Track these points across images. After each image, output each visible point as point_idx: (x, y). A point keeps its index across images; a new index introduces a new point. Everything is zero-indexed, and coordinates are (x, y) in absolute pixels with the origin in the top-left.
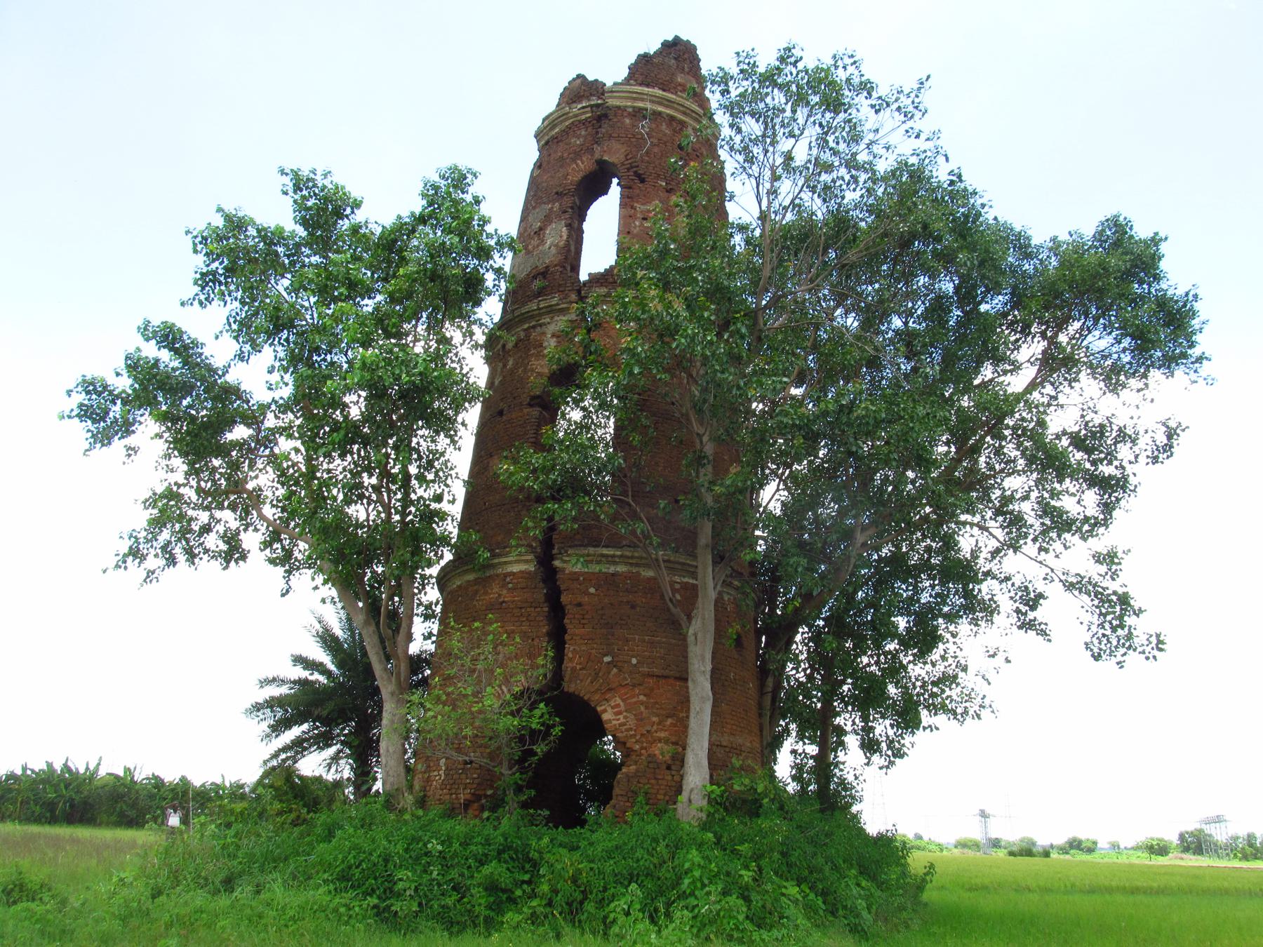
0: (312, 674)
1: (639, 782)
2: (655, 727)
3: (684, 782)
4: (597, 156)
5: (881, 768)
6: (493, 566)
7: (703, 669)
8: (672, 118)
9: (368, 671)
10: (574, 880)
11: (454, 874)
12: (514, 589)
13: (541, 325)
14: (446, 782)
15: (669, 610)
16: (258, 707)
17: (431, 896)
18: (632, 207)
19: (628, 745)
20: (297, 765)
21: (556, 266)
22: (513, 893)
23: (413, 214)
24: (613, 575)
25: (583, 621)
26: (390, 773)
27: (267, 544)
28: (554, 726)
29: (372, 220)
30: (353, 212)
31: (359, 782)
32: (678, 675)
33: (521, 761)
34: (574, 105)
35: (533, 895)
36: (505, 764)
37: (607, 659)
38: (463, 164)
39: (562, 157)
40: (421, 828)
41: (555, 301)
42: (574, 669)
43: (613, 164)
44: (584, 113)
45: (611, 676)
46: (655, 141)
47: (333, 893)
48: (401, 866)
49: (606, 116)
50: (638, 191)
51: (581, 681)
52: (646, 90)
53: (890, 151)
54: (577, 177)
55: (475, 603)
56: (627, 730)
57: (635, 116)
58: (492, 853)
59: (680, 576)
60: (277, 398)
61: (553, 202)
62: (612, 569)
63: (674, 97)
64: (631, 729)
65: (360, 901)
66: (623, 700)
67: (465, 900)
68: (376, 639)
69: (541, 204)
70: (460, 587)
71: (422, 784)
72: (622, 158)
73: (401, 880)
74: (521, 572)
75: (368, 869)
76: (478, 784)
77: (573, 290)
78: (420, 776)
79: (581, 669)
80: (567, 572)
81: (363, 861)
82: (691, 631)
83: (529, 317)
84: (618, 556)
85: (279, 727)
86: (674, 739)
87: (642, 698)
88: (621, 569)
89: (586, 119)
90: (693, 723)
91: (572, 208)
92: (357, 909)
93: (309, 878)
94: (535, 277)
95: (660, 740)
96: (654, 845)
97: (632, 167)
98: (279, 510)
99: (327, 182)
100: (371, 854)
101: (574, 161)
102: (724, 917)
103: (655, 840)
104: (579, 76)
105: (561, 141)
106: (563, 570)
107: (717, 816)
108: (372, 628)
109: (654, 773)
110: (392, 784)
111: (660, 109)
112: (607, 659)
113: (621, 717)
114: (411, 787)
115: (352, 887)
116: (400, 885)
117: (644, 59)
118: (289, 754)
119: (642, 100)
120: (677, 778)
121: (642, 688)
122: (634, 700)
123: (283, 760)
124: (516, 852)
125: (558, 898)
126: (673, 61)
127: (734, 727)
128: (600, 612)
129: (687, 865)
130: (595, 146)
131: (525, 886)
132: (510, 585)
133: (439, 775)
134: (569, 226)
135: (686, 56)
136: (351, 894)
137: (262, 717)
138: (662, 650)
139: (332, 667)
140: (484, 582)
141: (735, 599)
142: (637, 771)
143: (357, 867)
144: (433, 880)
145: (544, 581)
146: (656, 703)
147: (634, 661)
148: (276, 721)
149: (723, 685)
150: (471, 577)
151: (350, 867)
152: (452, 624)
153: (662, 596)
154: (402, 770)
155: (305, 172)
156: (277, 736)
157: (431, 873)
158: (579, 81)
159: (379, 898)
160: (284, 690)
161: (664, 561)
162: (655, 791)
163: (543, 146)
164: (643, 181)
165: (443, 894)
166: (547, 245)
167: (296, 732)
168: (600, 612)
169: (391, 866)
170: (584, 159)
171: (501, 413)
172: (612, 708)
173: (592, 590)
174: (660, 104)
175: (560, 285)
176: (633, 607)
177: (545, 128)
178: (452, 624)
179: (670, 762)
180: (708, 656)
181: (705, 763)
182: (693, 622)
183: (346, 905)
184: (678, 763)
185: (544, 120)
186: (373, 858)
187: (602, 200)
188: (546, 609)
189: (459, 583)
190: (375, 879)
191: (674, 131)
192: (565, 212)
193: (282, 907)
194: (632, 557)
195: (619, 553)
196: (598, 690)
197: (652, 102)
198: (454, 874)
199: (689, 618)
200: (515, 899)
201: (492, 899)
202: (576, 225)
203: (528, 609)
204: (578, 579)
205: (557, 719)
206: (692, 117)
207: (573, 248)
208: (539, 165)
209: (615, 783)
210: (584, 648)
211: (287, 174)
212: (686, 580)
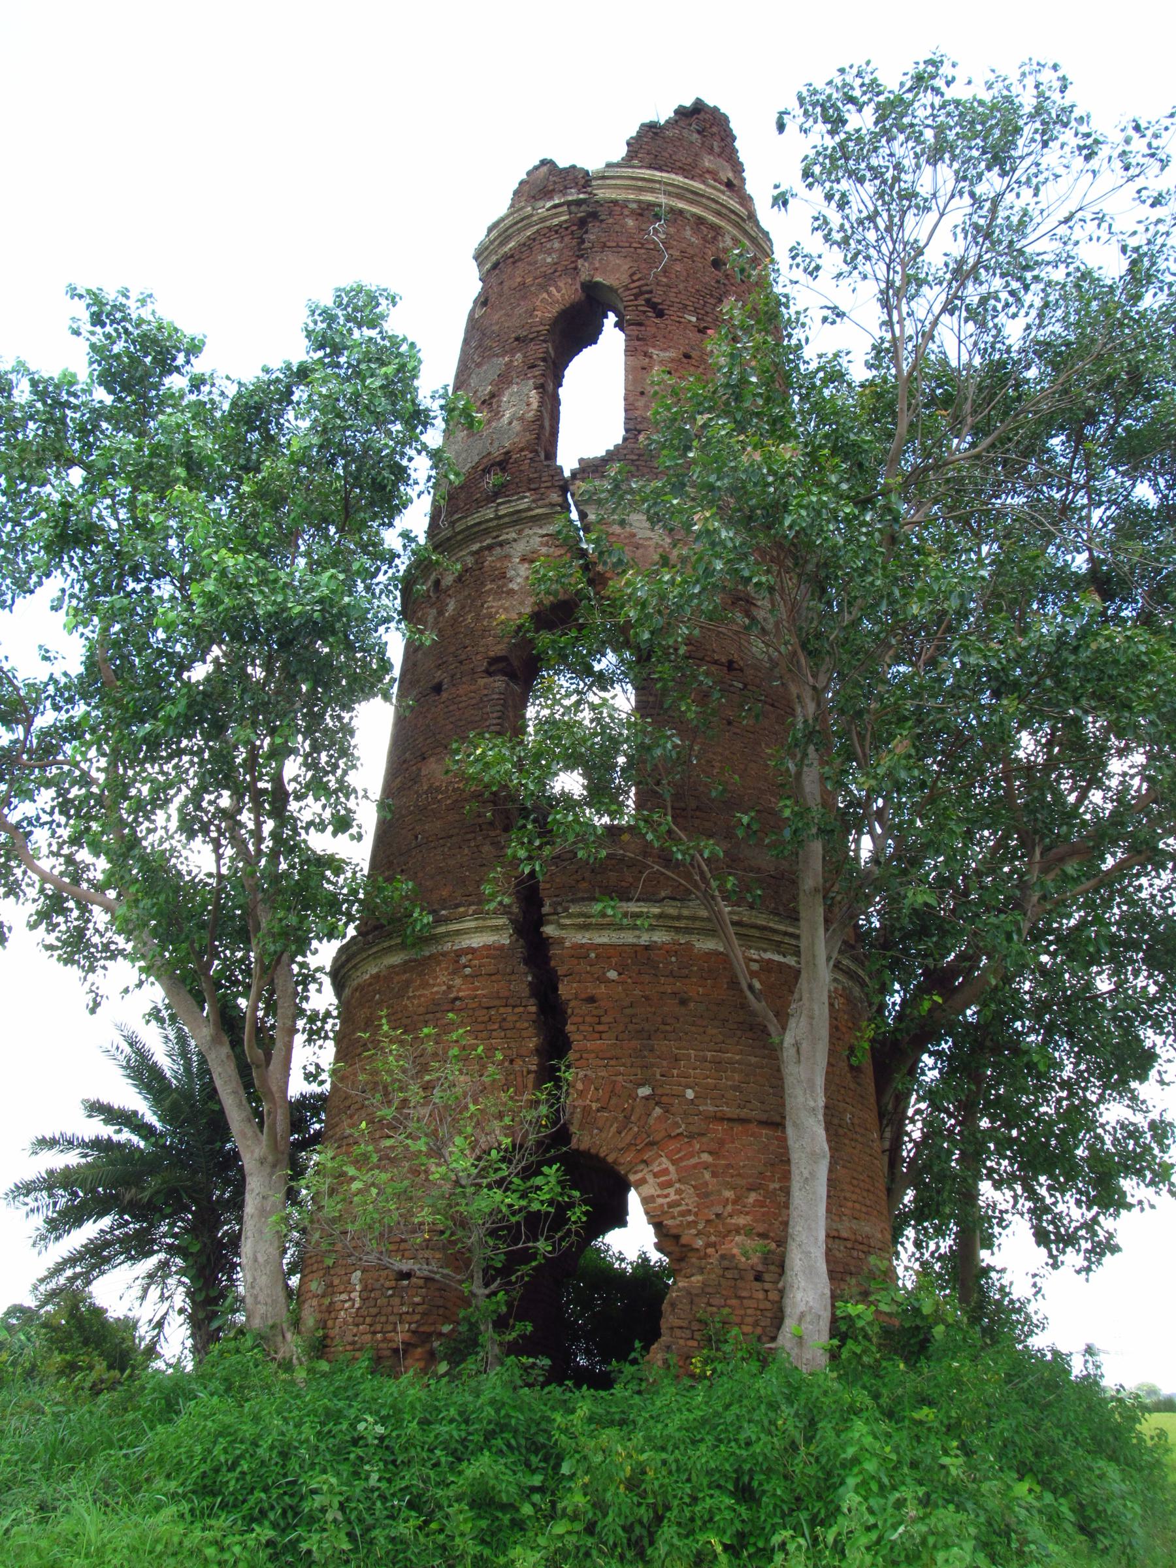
0: (120, 1131)
2: (729, 1208)
3: (787, 1302)
4: (584, 276)
5: (1078, 1272)
7: (812, 1104)
8: (700, 220)
9: (219, 1126)
10: (633, 1484)
11: (409, 1477)
12: (473, 976)
13: (501, 545)
16: (27, 1189)
17: (369, 1520)
18: (646, 354)
19: (683, 1240)
20: (91, 1288)
21: (522, 450)
22: (517, 1510)
23: (289, 367)
24: (647, 948)
25: (600, 1028)
26: (261, 1298)
27: (44, 916)
28: (570, 1206)
29: (221, 373)
30: (188, 362)
31: (201, 1315)
32: (764, 1117)
33: (506, 1271)
34: (541, 204)
35: (552, 1516)
36: (478, 1276)
37: (644, 1091)
38: (372, 282)
40: (335, 1394)
41: (524, 504)
42: (586, 1110)
43: (610, 289)
45: (651, 1121)
46: (677, 254)
47: (188, 1517)
48: (313, 1465)
49: (594, 215)
50: (654, 330)
52: (658, 174)
53: (1105, 225)
54: (553, 311)
56: (683, 1214)
58: (475, 1438)
59: (758, 949)
60: (58, 676)
61: (512, 352)
62: (645, 939)
65: (242, 1533)
66: (673, 1162)
67: (434, 1526)
68: (231, 1069)
69: (489, 357)
70: (376, 977)
71: (319, 1316)
72: (625, 279)
73: (314, 1492)
74: (487, 947)
75: (253, 1471)
76: (424, 1314)
77: (553, 486)
78: (315, 1302)
79: (598, 1110)
80: (567, 944)
81: (241, 1456)
82: (788, 1040)
83: (472, 535)
85: (60, 1224)
86: (761, 1228)
87: (706, 1157)
88: (660, 937)
89: (560, 225)
90: (798, 1196)
91: (544, 360)
92: (237, 1549)
93: (136, 1490)
94: (487, 470)
95: (738, 1231)
96: (772, 1415)
97: (642, 293)
98: (62, 860)
99: (145, 313)
100: (255, 1444)
101: (543, 288)
102: (935, 1546)
103: (773, 1406)
104: (544, 162)
105: (520, 260)
106: (560, 941)
107: (865, 1359)
108: (226, 1049)
109: (735, 1287)
110: (264, 1318)
111: (681, 205)
112: (644, 1091)
113: (671, 1191)
114: (296, 1323)
115: (224, 1506)
116: (318, 1501)
117: (650, 131)
118: (78, 1269)
119: (652, 191)
120: (773, 1296)
121: (704, 1139)
123: (68, 1279)
124: (515, 1432)
125: (610, 1519)
126: (696, 136)
127: (857, 1206)
128: (628, 1011)
129: (851, 1451)
130: (580, 262)
131: (536, 1498)
132: (468, 971)
133: (351, 1300)
134: (540, 387)
135: (714, 130)
136: (222, 1522)
137: (33, 1205)
138: (736, 1076)
139: (151, 1119)
140: (420, 967)
141: (844, 988)
142: (705, 1284)
143: (231, 1469)
144: (372, 1490)
145: (527, 961)
146: (729, 1166)
147: (690, 1094)
148: (59, 1213)
150: (396, 959)
151: (217, 1470)
152: (385, 1028)
153: (734, 983)
154: (281, 1295)
155: (111, 295)
156: (57, 1239)
157: (367, 1479)
158: (545, 169)
159: (275, 1525)
160: (73, 1159)
161: (734, 924)
163: (489, 271)
164: (660, 314)
165: (392, 1517)
166: (505, 420)
167: (90, 1230)
168: (628, 1011)
169: (294, 1465)
170: (561, 284)
171: (438, 689)
172: (656, 1175)
173: (612, 974)
174: (679, 197)
175: (530, 480)
176: (683, 1002)
177: (492, 242)
178: (385, 1028)
179: (760, 1268)
180: (820, 1081)
181: (822, 1267)
182: (792, 1023)
183: (216, 1543)
184: (772, 1268)
185: (490, 230)
186: (260, 1451)
187: (587, 353)
188: (533, 1009)
189: (374, 971)
190: (266, 1490)
191: (704, 239)
192: (533, 366)
193: (98, 1550)
194: (679, 918)
197: (669, 194)
198: (409, 1477)
200: (523, 1522)
201: (483, 1524)
202: (550, 388)
203: (502, 1010)
204: (587, 957)
205: (576, 1194)
206: (730, 221)
207: (547, 424)
208: (483, 301)
209: (665, 1306)
211: (81, 297)
212: (768, 956)
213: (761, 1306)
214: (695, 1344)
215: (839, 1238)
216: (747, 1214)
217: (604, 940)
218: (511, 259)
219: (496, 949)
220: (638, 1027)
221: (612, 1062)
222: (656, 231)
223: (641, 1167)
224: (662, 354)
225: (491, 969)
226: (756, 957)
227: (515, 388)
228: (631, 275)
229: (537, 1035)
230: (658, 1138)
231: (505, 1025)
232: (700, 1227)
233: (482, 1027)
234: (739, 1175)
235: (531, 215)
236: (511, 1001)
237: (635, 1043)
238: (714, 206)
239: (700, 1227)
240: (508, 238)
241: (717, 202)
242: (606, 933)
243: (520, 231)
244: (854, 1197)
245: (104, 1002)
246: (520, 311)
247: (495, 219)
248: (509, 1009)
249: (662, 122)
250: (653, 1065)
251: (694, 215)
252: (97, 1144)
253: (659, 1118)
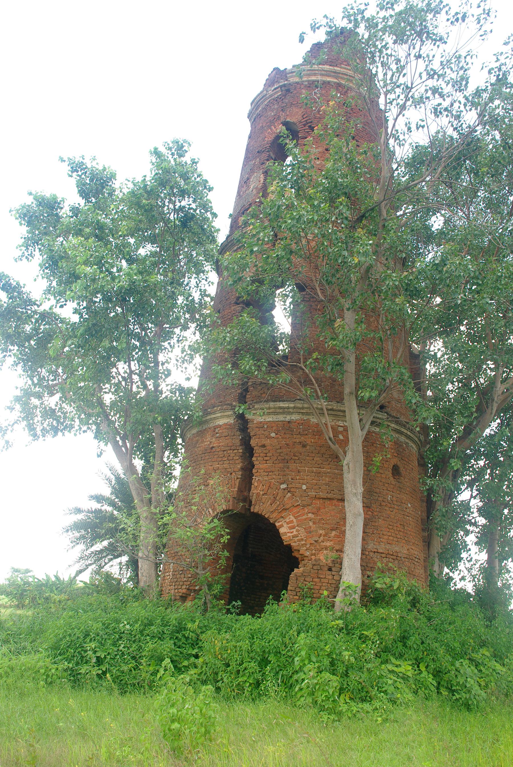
2: (322, 538)
6: (206, 422)
7: (354, 491)
14: (172, 580)
24: (289, 422)
25: (266, 458)
26: (144, 574)
37: (283, 486)
38: (181, 137)
39: (262, 127)
43: (293, 123)
45: (285, 499)
56: (299, 541)
57: (309, 87)
61: (255, 158)
62: (288, 418)
63: (339, 69)
66: (296, 518)
72: (300, 118)
74: (225, 424)
80: (255, 422)
82: (345, 462)
84: (291, 408)
87: (310, 515)
88: (295, 417)
89: (277, 97)
95: (326, 549)
104: (274, 69)
106: (252, 421)
110: (145, 582)
111: (329, 79)
112: (283, 486)
113: (294, 530)
119: (315, 75)
121: (310, 507)
122: (304, 517)
127: (391, 538)
149: (381, 505)
160: (80, 516)
161: (328, 410)
162: (318, 588)
172: (288, 523)
173: (273, 435)
177: (253, 109)
179: (331, 565)
180: (360, 481)
185: (251, 104)
188: (241, 451)
194: (303, 408)
195: (292, 405)
197: (322, 75)
199: (345, 453)
203: (229, 452)
211: (64, 161)
214: (297, 597)
216: (331, 541)
217: (271, 419)
218: (259, 116)
220: (283, 458)
221: (270, 474)
222: (315, 93)
223: (282, 519)
225: (226, 434)
226: (342, 425)
227: (255, 174)
229: (242, 462)
230: (288, 507)
231: (230, 458)
232: (308, 546)
234: (326, 523)
235: (266, 95)
238: (345, 77)
239: (308, 546)
240: (259, 106)
241: (347, 75)
242: (271, 416)
243: (262, 103)
244: (389, 534)
245: (104, 453)
248: (231, 451)
249: (323, 41)
251: (335, 83)
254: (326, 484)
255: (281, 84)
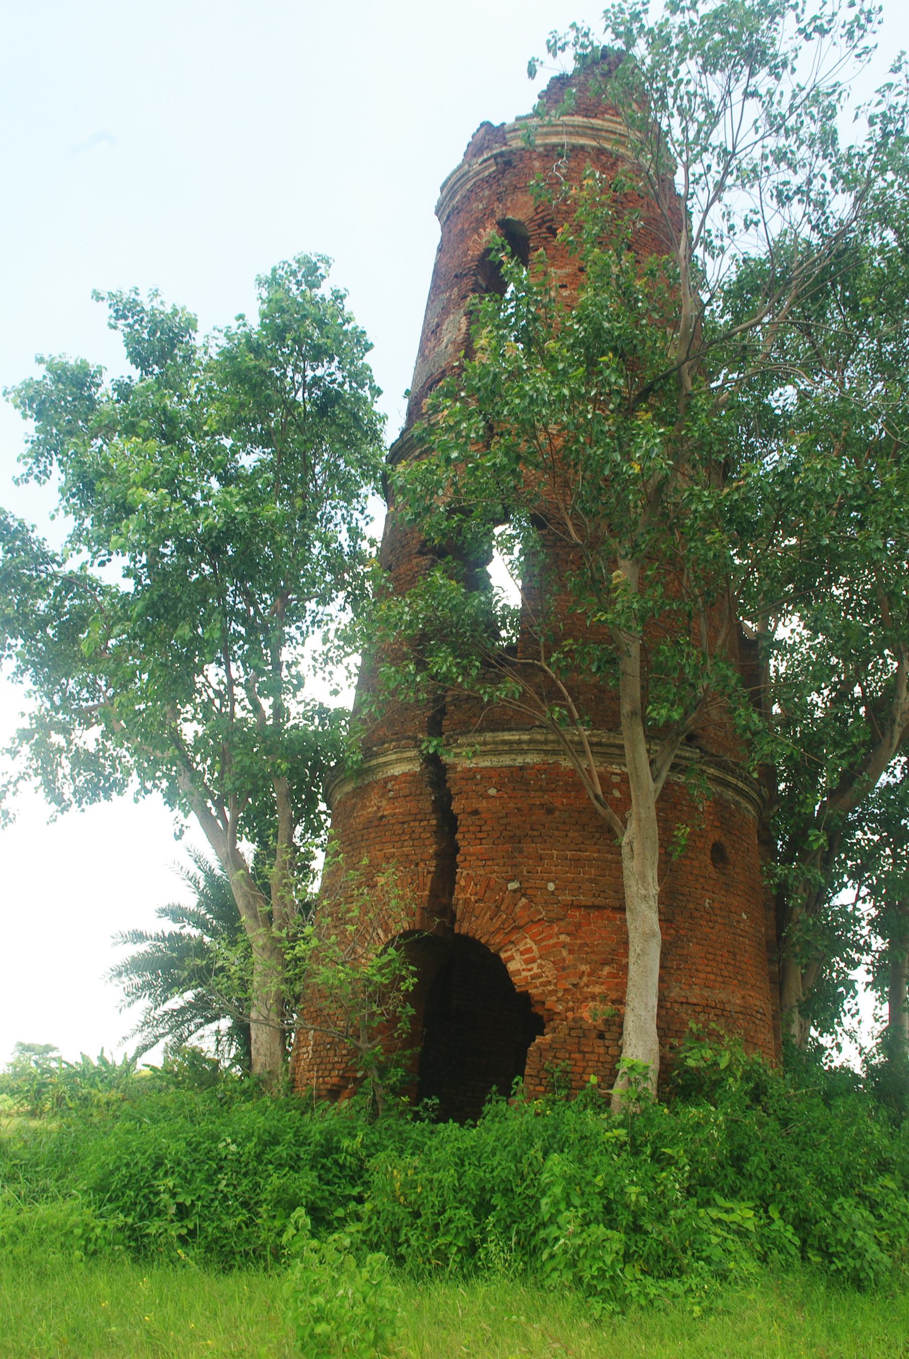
1: (555, 1057)
2: (585, 979)
4: (499, 216)
6: (371, 770)
7: (643, 892)
15: (596, 812)
19: (547, 1006)
24: (521, 768)
26: (262, 1051)
37: (513, 886)
43: (520, 223)
44: (489, 166)
45: (517, 909)
51: (477, 918)
55: (352, 821)
56: (543, 984)
57: (547, 156)
61: (451, 288)
62: (519, 761)
63: (600, 122)
64: (549, 983)
66: (537, 943)
74: (404, 774)
80: (459, 769)
82: (625, 840)
84: (525, 742)
87: (563, 937)
88: (531, 759)
89: (489, 176)
95: (594, 998)
97: (545, 222)
99: (156, 303)
104: (482, 125)
106: (454, 767)
110: (264, 1065)
111: (582, 141)
112: (513, 886)
113: (535, 966)
119: (557, 134)
121: (562, 923)
122: (552, 941)
127: (712, 977)
128: (504, 821)
132: (391, 794)
147: (551, 887)
149: (691, 917)
158: (483, 130)
160: (144, 947)
168: (504, 821)
172: (522, 953)
173: (492, 792)
176: (550, 811)
177: (444, 199)
179: (602, 1028)
185: (442, 190)
188: (434, 822)
194: (546, 742)
195: (526, 737)
196: (499, 929)
197: (570, 134)
199: (625, 822)
203: (412, 824)
210: (481, 872)
213: (602, 1059)
215: (687, 1003)
216: (602, 984)
217: (488, 764)
218: (457, 210)
219: (411, 775)
221: (489, 863)
224: (559, 271)
226: (618, 771)
228: (536, 209)
233: (397, 838)
234: (593, 952)
235: (468, 172)
236: (419, 817)
237: (508, 847)
238: (612, 136)
239: (560, 994)
240: (455, 193)
241: (615, 133)
242: (488, 758)
243: (462, 186)
246: (458, 253)
247: (443, 180)
248: (417, 824)
249: (570, 73)
250: (521, 864)
251: (593, 148)
252: (175, 938)
253: (524, 907)
254: (591, 881)
255: (495, 152)
